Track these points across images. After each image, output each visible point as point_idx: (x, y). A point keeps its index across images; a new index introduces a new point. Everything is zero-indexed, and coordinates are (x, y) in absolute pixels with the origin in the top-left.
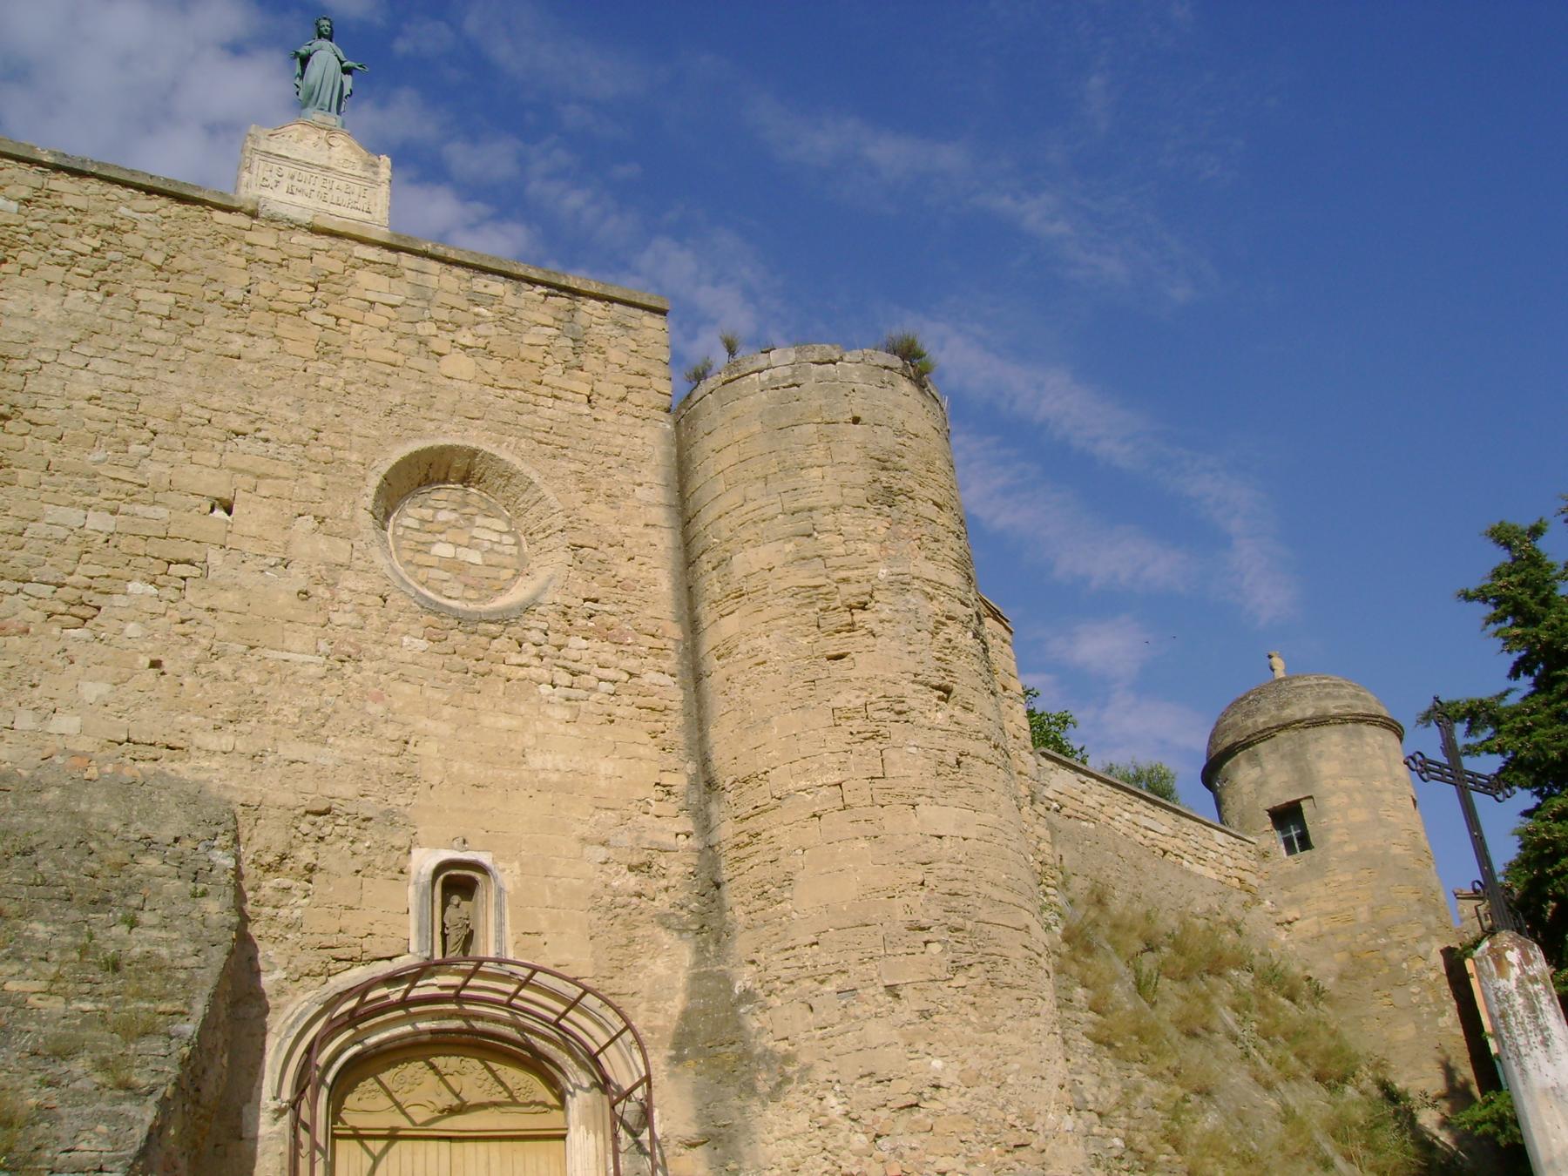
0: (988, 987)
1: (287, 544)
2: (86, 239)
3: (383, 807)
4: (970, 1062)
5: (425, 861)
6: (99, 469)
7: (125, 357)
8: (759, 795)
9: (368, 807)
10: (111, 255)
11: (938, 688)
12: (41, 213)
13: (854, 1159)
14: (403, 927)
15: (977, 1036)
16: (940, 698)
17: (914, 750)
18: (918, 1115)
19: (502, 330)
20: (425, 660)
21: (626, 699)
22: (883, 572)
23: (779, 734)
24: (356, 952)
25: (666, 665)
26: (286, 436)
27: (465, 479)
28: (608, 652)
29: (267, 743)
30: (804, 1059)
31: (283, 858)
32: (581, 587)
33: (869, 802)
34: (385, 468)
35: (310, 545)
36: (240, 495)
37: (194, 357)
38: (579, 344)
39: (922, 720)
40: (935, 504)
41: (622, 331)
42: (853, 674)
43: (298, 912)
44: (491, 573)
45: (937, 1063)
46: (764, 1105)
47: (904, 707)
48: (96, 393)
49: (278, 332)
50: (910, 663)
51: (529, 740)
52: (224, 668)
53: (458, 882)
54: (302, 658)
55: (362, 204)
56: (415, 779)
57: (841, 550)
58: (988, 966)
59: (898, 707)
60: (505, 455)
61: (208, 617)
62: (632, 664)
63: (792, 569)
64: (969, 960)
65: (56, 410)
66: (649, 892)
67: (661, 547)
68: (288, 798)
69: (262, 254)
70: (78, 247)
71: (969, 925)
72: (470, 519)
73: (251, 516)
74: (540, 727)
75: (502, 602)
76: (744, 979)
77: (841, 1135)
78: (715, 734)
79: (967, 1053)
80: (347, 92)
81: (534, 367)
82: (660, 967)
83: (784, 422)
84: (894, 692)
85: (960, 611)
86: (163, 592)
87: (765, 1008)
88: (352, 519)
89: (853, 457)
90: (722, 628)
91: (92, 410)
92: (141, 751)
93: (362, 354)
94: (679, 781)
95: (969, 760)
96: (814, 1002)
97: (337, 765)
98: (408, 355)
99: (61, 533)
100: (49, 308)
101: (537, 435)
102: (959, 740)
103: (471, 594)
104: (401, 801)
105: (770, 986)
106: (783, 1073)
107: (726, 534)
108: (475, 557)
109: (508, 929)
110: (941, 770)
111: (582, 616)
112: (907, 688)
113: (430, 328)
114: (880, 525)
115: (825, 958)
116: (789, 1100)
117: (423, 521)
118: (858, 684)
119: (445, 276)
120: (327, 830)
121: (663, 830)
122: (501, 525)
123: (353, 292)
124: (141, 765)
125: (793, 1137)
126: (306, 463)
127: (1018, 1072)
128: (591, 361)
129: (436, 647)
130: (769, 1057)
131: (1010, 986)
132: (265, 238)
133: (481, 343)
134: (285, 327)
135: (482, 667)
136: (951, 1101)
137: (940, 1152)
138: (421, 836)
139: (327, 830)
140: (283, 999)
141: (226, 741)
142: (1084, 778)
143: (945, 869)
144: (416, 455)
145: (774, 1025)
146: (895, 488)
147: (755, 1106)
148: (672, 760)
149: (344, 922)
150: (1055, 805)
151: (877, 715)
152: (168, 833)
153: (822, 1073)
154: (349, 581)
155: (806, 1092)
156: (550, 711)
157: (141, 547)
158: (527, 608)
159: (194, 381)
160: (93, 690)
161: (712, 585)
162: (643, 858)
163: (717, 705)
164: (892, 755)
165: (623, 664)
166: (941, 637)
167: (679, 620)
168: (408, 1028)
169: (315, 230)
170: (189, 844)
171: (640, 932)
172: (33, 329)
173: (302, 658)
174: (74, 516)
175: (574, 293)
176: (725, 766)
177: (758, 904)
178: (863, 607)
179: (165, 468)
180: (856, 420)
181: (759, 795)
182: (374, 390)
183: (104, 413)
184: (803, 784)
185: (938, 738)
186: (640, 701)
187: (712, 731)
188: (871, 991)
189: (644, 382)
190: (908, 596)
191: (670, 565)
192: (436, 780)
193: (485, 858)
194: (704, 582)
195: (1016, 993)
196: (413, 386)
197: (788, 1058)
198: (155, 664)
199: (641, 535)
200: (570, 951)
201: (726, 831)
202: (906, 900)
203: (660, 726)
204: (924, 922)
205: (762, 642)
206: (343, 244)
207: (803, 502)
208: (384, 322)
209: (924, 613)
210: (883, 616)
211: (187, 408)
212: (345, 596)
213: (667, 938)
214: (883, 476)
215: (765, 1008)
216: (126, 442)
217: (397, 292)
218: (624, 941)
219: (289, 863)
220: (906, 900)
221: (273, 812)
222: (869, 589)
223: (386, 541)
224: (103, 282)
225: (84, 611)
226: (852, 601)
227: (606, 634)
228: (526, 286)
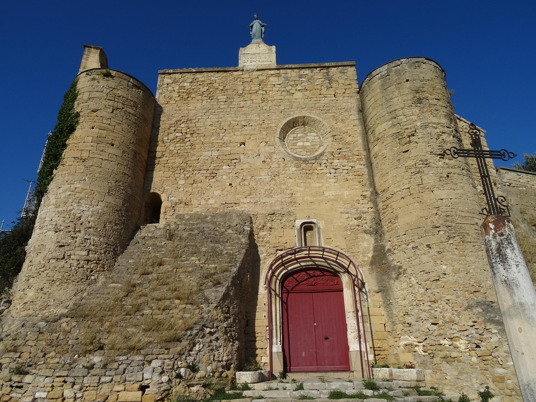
0: (461, 243)
1: (259, 150)
2: (205, 88)
3: (288, 210)
4: (456, 266)
5: (298, 223)
6: (214, 141)
7: (217, 114)
8: (387, 194)
9: (285, 211)
10: (211, 90)
11: (439, 155)
12: (195, 84)
13: (421, 296)
14: (292, 239)
15: (458, 258)
16: (440, 158)
17: (432, 175)
18: (439, 283)
19: (309, 83)
20: (296, 173)
21: (351, 174)
22: (419, 124)
23: (393, 178)
24: (283, 247)
25: (362, 163)
26: (256, 124)
27: (304, 124)
28: (345, 162)
29: (258, 199)
30: (404, 267)
31: (264, 226)
32: (336, 146)
33: (418, 192)
34: (281, 126)
35: (265, 149)
36: (247, 140)
37: (233, 110)
38: (330, 81)
39: (434, 165)
40: (436, 99)
41: (343, 74)
42: (410, 156)
43: (268, 239)
44: (313, 147)
45: (444, 267)
46: (395, 281)
47: (428, 162)
48: (211, 123)
49: (251, 98)
50: (429, 149)
51: (325, 189)
52: (246, 183)
53: (307, 227)
54: (264, 177)
55: (269, 60)
56: (295, 203)
57: (405, 120)
58: (461, 237)
59: (425, 163)
60: (312, 116)
61: (241, 171)
62: (352, 164)
63: (391, 129)
64: (454, 235)
65: (203, 129)
66: (361, 225)
67: (358, 131)
68: (263, 212)
69: (246, 80)
70: (204, 90)
71: (453, 225)
72: (306, 134)
73: (250, 145)
74: (327, 185)
75: (316, 154)
76: (388, 246)
77: (416, 289)
78: (376, 179)
79: (455, 263)
80: (263, 32)
81: (319, 90)
82: (365, 244)
83: (386, 87)
84: (424, 158)
85: (446, 130)
86: (231, 167)
87: (394, 253)
88: (274, 141)
89: (407, 92)
90: (375, 150)
91: (211, 128)
92: (229, 205)
93: (273, 99)
94: (368, 194)
95: (452, 175)
96: (406, 251)
97: (276, 202)
98: (285, 96)
99: (207, 158)
100: (199, 105)
101: (321, 108)
102: (448, 169)
103: (308, 154)
104: (292, 209)
105: (394, 247)
106: (400, 271)
107: (373, 123)
108: (308, 144)
109: (322, 238)
110: (441, 179)
111: (339, 153)
112: (429, 156)
113: (290, 87)
114: (416, 110)
115: (408, 238)
116: (401, 279)
117: (294, 137)
118: (412, 158)
119: (292, 73)
120: (274, 218)
121: (364, 207)
122: (315, 134)
123: (269, 83)
124: (229, 208)
125: (403, 290)
126: (262, 129)
127: (474, 269)
128: (334, 85)
129: (298, 169)
130: (395, 267)
131: (470, 242)
132: (246, 76)
133: (304, 88)
134: (253, 97)
135: (311, 172)
136: (450, 278)
137: (447, 293)
138: (298, 217)
139: (274, 218)
140: (265, 261)
141: (248, 200)
142: (520, 174)
143: (444, 209)
144: (289, 121)
145: (397, 258)
146: (422, 98)
147: (392, 281)
148: (366, 188)
149: (280, 240)
150: (508, 184)
151: (419, 166)
152: (234, 224)
153: (409, 271)
154: (275, 156)
155: (405, 277)
156: (330, 180)
157: (225, 157)
158: (321, 155)
159: (233, 115)
160: (217, 193)
161: (372, 138)
162: (358, 215)
163: (375, 171)
164: (424, 177)
165: (349, 165)
166: (440, 139)
167: (365, 150)
168: (298, 265)
169: (258, 70)
170: (239, 225)
171: (359, 236)
172: (196, 112)
173: (264, 177)
174: (209, 153)
175: (328, 67)
176: (379, 189)
177: (390, 224)
178: (413, 135)
179: (229, 138)
180: (407, 81)
181: (387, 194)
182: (277, 107)
183: (213, 128)
184: (398, 189)
185: (440, 170)
186: (355, 174)
187: (375, 179)
188: (422, 247)
189: (350, 86)
190: (428, 129)
191: (361, 135)
192: (300, 202)
193: (314, 221)
194: (370, 138)
195: (472, 244)
196: (287, 104)
197: (400, 267)
198: (230, 184)
199: (352, 129)
200: (338, 243)
201: (381, 205)
202: (431, 219)
203: (362, 179)
204: (438, 225)
205: (384, 151)
206: (266, 72)
207: (393, 109)
208: (278, 89)
209: (433, 133)
210: (419, 137)
211: (232, 122)
212: (274, 160)
213: (367, 237)
214: (417, 95)
215: (394, 253)
216: (219, 134)
217: (281, 80)
218: (354, 238)
219: (265, 227)
220: (431, 219)
221: (260, 215)
222: (414, 130)
223: (285, 144)
224: (210, 97)
225: (213, 175)
226: (409, 134)
227: (344, 157)
228: (314, 69)
